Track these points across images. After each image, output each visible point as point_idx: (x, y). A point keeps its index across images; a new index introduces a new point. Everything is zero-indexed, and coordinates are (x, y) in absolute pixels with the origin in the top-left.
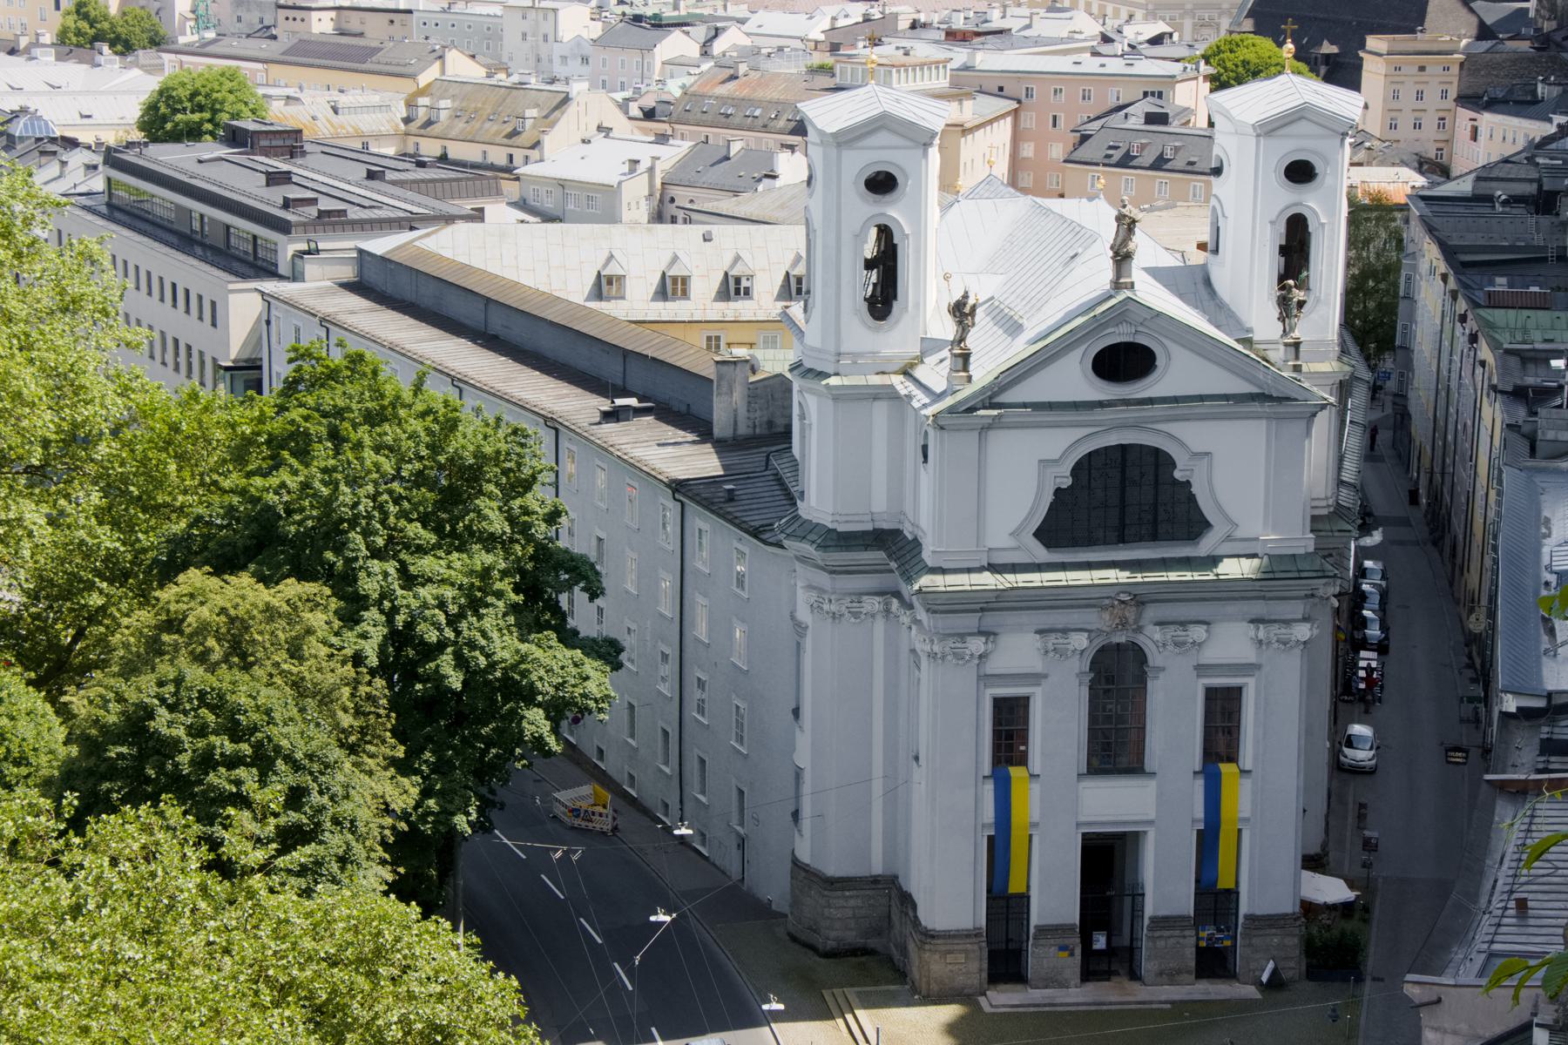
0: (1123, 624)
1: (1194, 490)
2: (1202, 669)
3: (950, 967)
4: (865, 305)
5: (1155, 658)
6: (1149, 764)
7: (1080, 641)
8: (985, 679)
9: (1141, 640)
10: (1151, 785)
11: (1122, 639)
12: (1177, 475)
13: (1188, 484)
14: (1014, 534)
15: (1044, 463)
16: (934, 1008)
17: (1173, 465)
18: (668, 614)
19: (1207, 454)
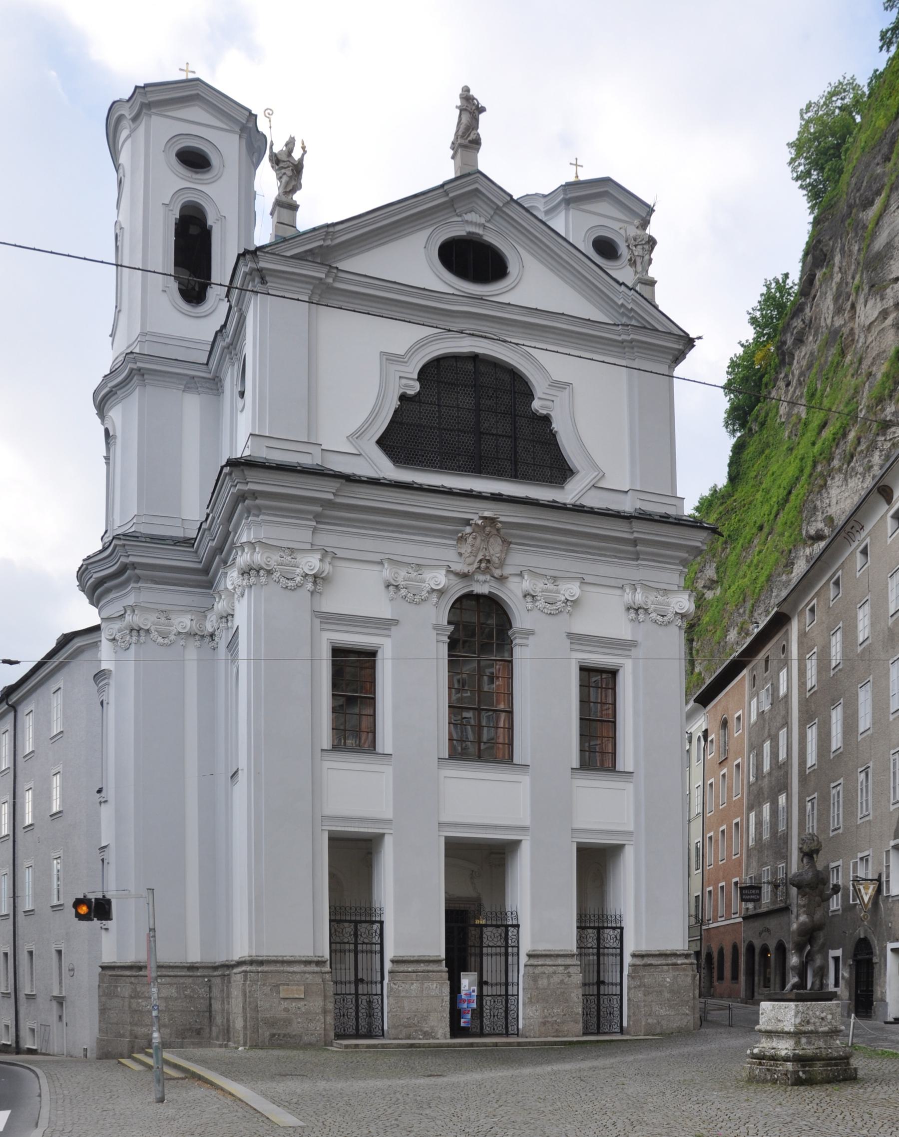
0: (486, 566)
1: (556, 426)
2: (576, 639)
3: (285, 1004)
12: (536, 405)
13: (546, 420)
14: (356, 436)
15: (389, 358)
17: (529, 395)
19: (569, 384)
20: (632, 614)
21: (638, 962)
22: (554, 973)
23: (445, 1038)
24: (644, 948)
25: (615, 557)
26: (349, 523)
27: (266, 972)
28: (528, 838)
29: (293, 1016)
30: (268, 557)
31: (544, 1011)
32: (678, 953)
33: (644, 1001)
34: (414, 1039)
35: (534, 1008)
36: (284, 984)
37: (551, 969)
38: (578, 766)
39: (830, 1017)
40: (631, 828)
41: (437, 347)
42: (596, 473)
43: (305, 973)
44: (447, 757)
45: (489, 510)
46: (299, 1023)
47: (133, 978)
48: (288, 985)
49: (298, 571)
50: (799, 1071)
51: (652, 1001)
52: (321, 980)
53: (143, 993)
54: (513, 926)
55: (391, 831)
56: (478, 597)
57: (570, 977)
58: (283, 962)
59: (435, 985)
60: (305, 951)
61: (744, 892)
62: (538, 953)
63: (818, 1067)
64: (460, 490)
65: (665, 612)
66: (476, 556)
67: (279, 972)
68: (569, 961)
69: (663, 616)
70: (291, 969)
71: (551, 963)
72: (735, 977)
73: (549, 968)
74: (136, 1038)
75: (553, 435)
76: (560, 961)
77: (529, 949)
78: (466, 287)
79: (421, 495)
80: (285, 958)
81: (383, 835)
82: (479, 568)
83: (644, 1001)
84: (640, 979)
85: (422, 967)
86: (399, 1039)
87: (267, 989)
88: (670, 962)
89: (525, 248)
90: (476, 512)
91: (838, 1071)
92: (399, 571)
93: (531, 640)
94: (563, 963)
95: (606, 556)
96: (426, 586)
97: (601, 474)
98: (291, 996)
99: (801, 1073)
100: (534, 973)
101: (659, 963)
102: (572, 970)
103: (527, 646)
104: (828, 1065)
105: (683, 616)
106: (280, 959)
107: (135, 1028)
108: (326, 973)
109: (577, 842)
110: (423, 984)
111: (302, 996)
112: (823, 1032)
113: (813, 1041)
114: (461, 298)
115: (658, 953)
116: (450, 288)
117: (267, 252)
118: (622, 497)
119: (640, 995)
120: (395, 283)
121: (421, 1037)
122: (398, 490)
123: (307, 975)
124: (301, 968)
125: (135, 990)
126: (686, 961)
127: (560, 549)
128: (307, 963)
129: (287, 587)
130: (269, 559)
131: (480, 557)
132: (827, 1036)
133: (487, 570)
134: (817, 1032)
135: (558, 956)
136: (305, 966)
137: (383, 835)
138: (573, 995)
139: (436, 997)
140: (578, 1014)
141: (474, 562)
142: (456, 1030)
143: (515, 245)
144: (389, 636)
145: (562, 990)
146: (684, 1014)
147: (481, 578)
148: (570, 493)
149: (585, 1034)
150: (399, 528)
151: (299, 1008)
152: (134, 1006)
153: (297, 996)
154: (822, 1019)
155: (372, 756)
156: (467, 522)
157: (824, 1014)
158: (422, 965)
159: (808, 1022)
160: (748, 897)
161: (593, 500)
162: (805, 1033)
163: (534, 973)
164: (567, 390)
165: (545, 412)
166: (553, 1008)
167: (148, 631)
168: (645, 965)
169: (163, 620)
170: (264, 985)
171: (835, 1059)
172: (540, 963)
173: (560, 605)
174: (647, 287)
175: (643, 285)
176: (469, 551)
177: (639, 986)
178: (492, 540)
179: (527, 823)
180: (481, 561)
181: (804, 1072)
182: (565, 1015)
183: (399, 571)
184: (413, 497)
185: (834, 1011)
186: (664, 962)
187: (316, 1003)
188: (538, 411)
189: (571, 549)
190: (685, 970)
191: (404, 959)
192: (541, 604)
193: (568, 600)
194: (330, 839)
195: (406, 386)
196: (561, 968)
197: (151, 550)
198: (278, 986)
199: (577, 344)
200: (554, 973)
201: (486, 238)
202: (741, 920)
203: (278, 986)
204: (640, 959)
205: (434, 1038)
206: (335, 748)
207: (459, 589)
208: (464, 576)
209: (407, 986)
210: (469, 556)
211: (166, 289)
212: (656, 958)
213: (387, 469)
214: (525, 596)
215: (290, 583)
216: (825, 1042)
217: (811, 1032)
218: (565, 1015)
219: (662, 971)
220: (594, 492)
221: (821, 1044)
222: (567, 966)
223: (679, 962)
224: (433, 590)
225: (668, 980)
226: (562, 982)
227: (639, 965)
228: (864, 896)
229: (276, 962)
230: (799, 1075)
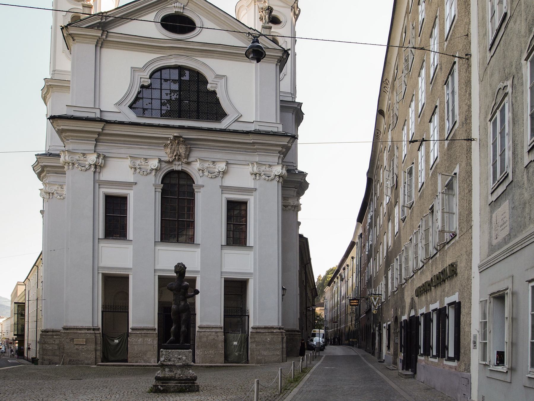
0: (178, 158)
1: (218, 96)
2: (224, 189)
3: (77, 347)
4: (43, 84)
5: (198, 180)
6: (198, 238)
7: (154, 163)
8: (98, 183)
9: (190, 170)
10: (199, 250)
11: (179, 168)
12: (209, 87)
13: (214, 93)
14: (119, 104)
15: (134, 70)
16: (240, 42)
17: (207, 82)
18: (10, 321)
19: (224, 76)
20: (253, 176)
21: (254, 331)
22: (210, 335)
23: (155, 363)
24: (257, 324)
25: (246, 152)
26: (112, 141)
27: (68, 333)
28: (200, 276)
29: (80, 352)
30: (133, 162)
31: (204, 352)
32: (274, 327)
33: (256, 348)
34: (140, 363)
35: (199, 350)
36: (76, 338)
37: (209, 333)
38: (104, 238)
39: (184, 358)
40: (252, 271)
41: (159, 63)
42: (237, 115)
43: (86, 333)
44: (160, 241)
45: (176, 133)
46: (83, 355)
47: (44, 336)
48: (78, 338)
49: (87, 163)
50: (158, 385)
51: (260, 349)
52: (94, 337)
53: (47, 342)
54: (192, 314)
55: (132, 273)
56: (178, 172)
57: (218, 337)
58: (77, 329)
59: (150, 340)
60: (151, 326)
61: (351, 301)
62: (203, 326)
63: (172, 384)
64: (220, 129)
65: (270, 175)
66: (173, 154)
67: (75, 333)
68: (218, 330)
69: (269, 177)
70: (82, 332)
71: (208, 331)
72: (365, 340)
73: (207, 333)
74: (45, 360)
75: (217, 100)
76: (213, 330)
77: (199, 324)
78: (174, 36)
79: (148, 128)
80: (78, 327)
81: (249, 279)
82: (175, 159)
83: (256, 348)
84: (254, 338)
85: (145, 332)
86: (132, 363)
87: (68, 340)
88: (270, 331)
89: (202, 16)
90: (171, 134)
91: (185, 386)
92: (136, 162)
93: (202, 190)
94: (215, 331)
95: (240, 151)
96: (149, 168)
97: (240, 115)
98: (79, 343)
99: (159, 387)
100: (200, 335)
101: (264, 331)
102: (219, 334)
103: (200, 192)
104: (179, 383)
105: (279, 176)
106: (76, 327)
107: (44, 356)
108: (97, 334)
109: (158, 275)
110: (144, 339)
111: (85, 343)
112: (180, 366)
113: (174, 370)
114: (170, 41)
115: (264, 327)
116: (165, 37)
117: (73, 26)
118: (251, 124)
119: (254, 346)
120: (136, 36)
121: (143, 362)
122: (87, 122)
123: (88, 335)
124: (86, 331)
125: (44, 341)
126: (279, 331)
127: (217, 149)
128: (89, 329)
129: (82, 170)
130: (134, 163)
131: (175, 154)
132: (183, 368)
133: (179, 159)
134: (175, 366)
135: (213, 328)
136: (88, 331)
137: (249, 279)
138: (219, 345)
139: (151, 345)
140: (222, 353)
141: (173, 156)
142: (227, 358)
143: (199, 16)
144: (132, 190)
145: (214, 343)
146: (277, 355)
147: (177, 163)
148: (223, 124)
149: (225, 363)
150: (137, 143)
151: (83, 349)
152: (44, 347)
153: (82, 343)
154: (179, 359)
155: (125, 241)
156: (167, 139)
157: (181, 356)
158: (145, 331)
159: (170, 360)
160: (352, 304)
161: (236, 127)
162: (167, 365)
163: (200, 335)
164: (224, 79)
165: (213, 89)
166: (209, 351)
167: (53, 194)
168: (257, 332)
169: (60, 189)
170: (67, 338)
171: (184, 380)
172: (203, 331)
173: (216, 174)
174: (267, 29)
175: (265, 29)
176: (170, 151)
177: (254, 342)
178: (180, 146)
179: (199, 269)
180: (175, 156)
181: (161, 386)
182: (215, 354)
183: (136, 162)
184: (141, 129)
185: (187, 355)
186: (267, 331)
187: (91, 347)
188: (209, 89)
189: (223, 149)
190: (277, 335)
191: (136, 328)
192: (206, 173)
193: (220, 172)
194: (225, 281)
195: (143, 81)
196: (214, 333)
197: (51, 160)
198: (73, 339)
199: (242, 59)
200: (210, 335)
201: (184, 14)
202: (365, 314)
203: (73, 339)
204: (255, 329)
205: (149, 362)
206: (228, 244)
207: (167, 168)
208: (169, 162)
209: (136, 340)
210: (170, 154)
211: (64, 51)
212: (263, 329)
213: (132, 117)
214: (199, 170)
215: (83, 168)
216: (182, 371)
217: (171, 365)
218: (215, 354)
219: (265, 335)
220: (236, 124)
221: (179, 372)
222: (216, 332)
223: (275, 331)
224: (153, 169)
225: (268, 339)
226: (214, 339)
227: (253, 332)
228: (374, 302)
229: (74, 329)
230: (158, 388)
